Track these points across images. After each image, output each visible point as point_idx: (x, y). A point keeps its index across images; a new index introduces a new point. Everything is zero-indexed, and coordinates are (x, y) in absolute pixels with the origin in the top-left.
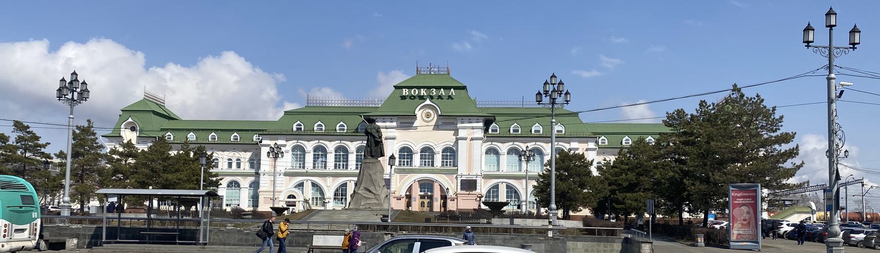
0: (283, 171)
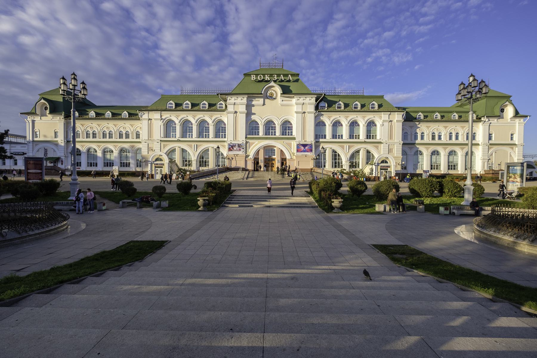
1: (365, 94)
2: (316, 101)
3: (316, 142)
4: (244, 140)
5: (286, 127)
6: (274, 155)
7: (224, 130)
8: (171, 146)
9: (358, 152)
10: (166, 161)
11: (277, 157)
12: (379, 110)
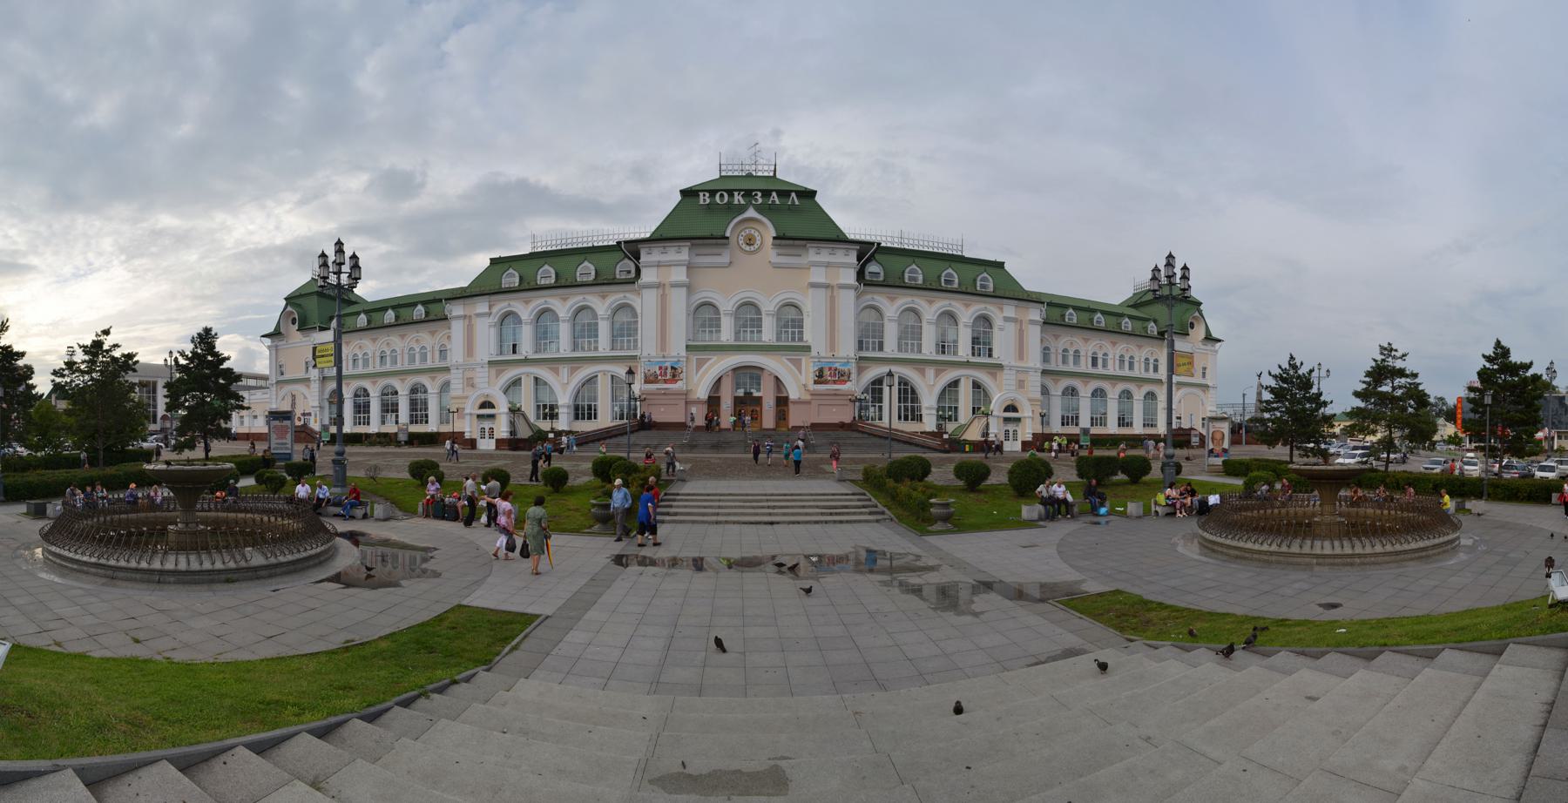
0: (486, 360)
1: (967, 255)
2: (859, 259)
5: (791, 318)
8: (511, 373)
9: (955, 384)
10: (502, 407)
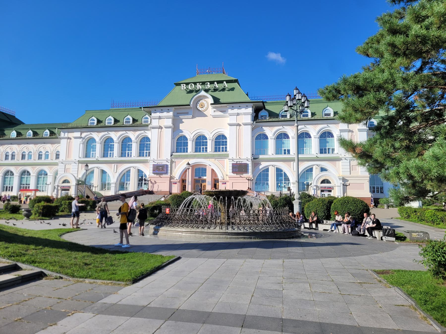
3: (254, 159)
4: (169, 158)
5: (220, 141)
6: (205, 176)
7: (148, 147)
9: (310, 170)
11: (208, 178)
12: (116, 125)
